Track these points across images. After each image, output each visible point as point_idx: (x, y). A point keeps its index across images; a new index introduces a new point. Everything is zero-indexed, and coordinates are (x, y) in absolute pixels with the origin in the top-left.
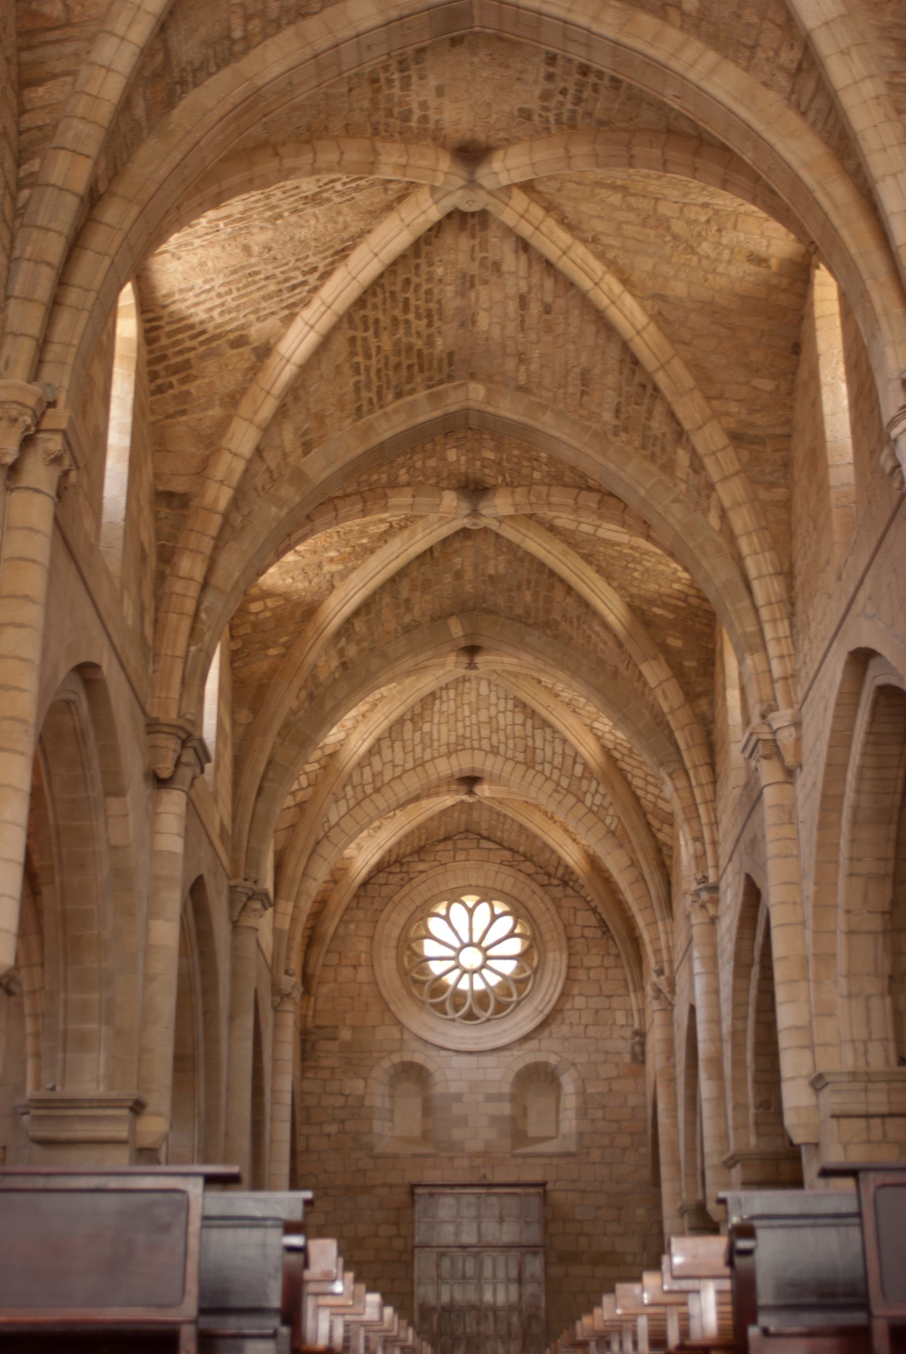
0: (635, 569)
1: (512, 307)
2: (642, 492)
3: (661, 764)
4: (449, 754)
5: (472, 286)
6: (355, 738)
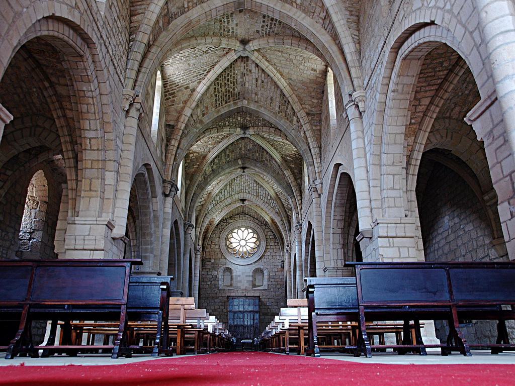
1: (254, 81)
5: (244, 76)
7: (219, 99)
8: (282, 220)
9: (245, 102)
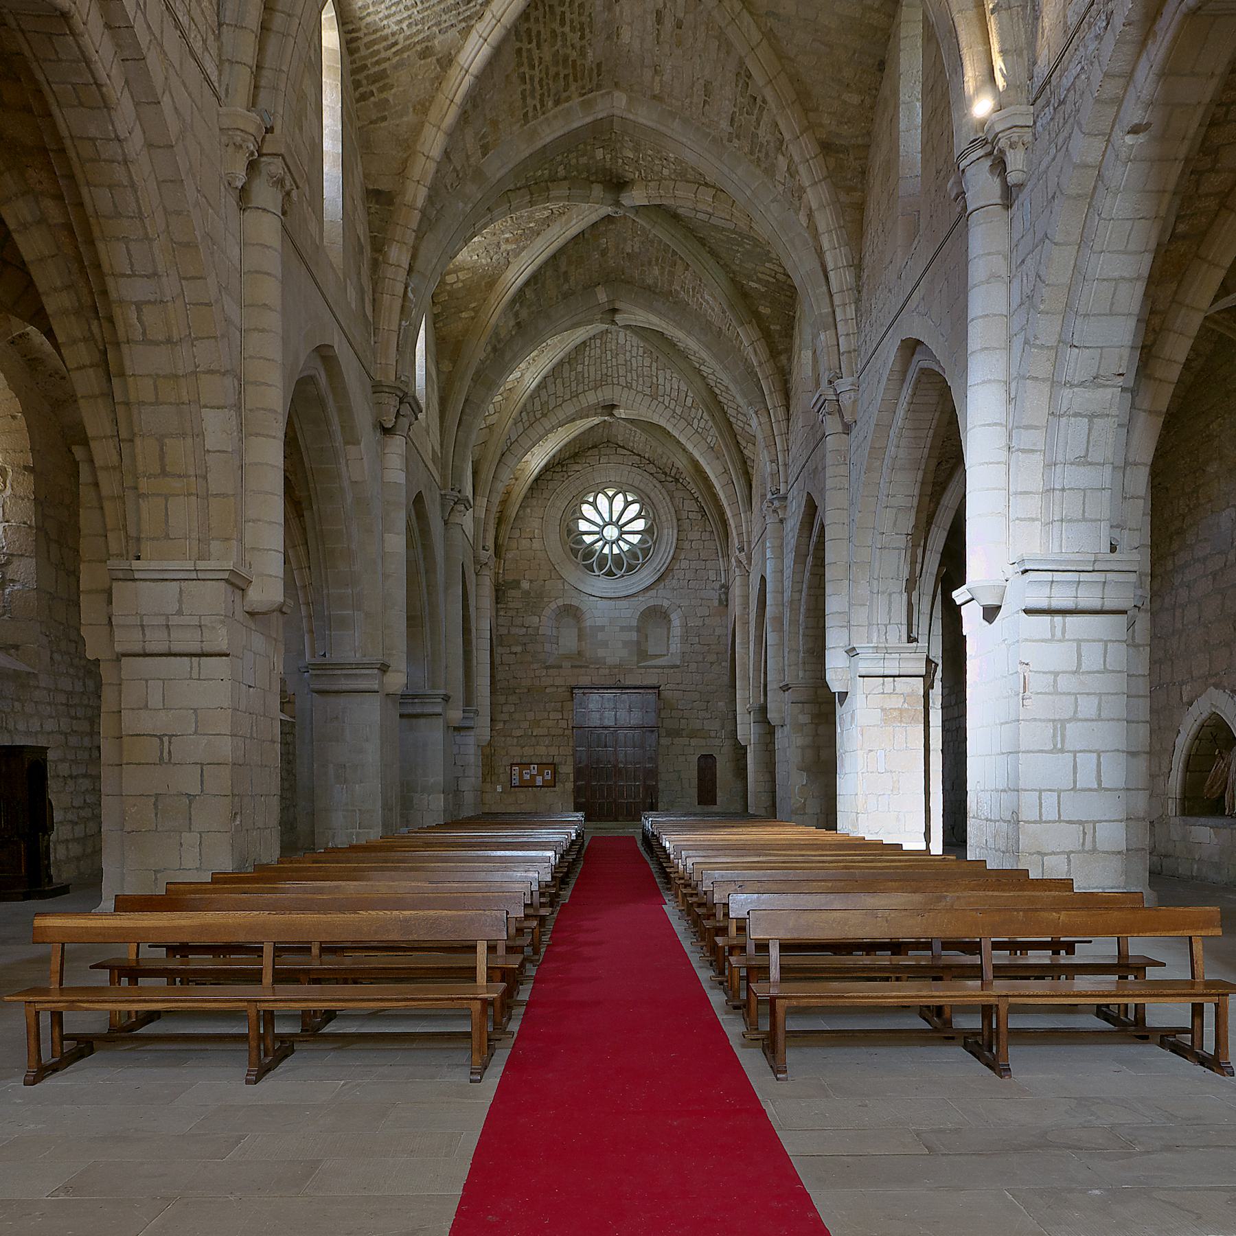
0: (738, 251)
1: (651, 20)
2: (748, 193)
3: (750, 404)
4: (596, 389)
6: (528, 376)
7: (533, 90)
8: (726, 471)
9: (621, 99)
